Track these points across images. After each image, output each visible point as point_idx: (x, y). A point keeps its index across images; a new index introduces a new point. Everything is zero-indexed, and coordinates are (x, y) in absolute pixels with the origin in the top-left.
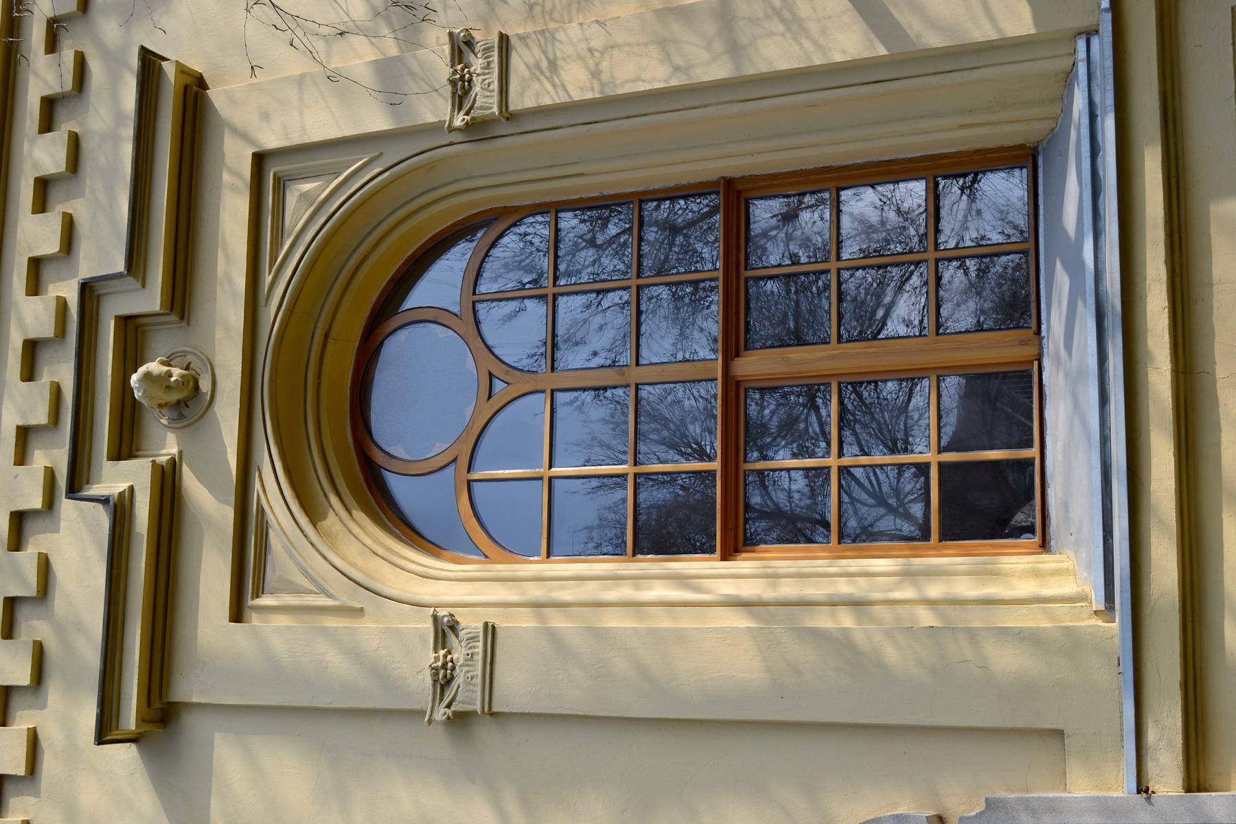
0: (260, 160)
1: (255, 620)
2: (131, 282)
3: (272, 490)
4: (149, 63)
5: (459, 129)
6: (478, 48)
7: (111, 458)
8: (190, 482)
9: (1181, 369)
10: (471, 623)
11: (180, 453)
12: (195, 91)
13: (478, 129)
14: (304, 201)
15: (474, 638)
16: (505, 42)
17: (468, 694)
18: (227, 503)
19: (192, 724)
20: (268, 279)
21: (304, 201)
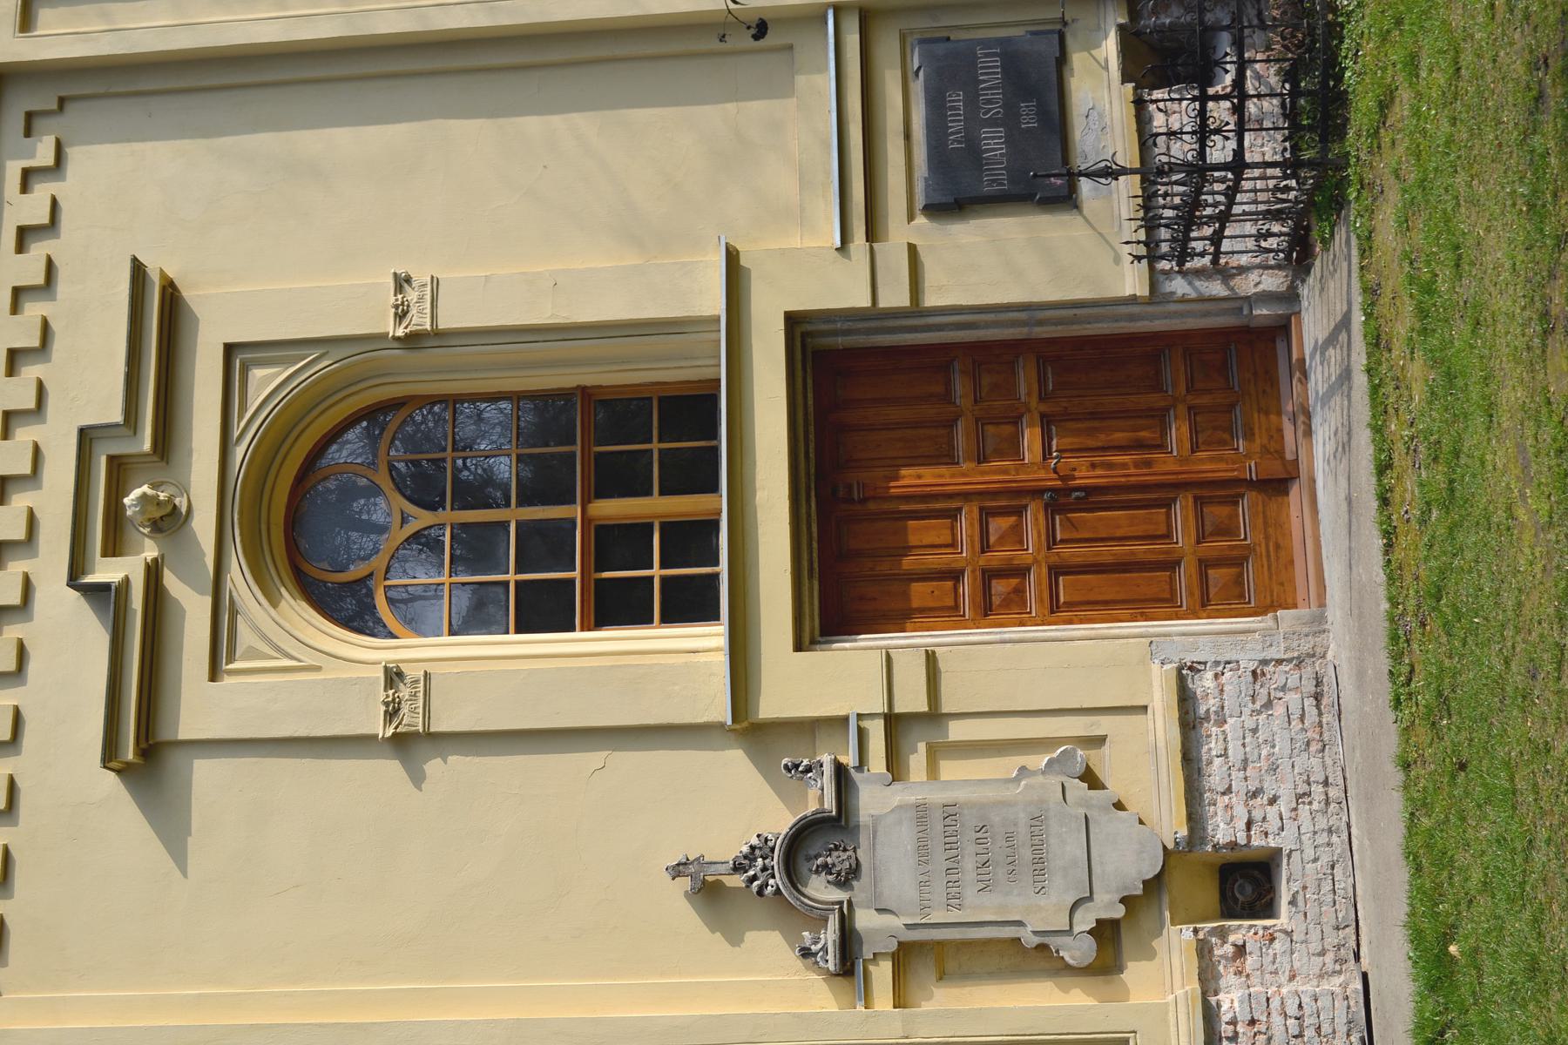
0: (230, 349)
1: (228, 681)
2: (125, 431)
3: (238, 578)
4: (138, 272)
5: (398, 339)
6: (408, 680)
7: (104, 555)
8: (170, 580)
9: (1301, 418)
10: (421, 276)
11: (163, 556)
12: (172, 297)
13: (413, 340)
14: (264, 381)
15: (417, 681)
16: (435, 283)
17: (411, 720)
18: (202, 593)
19: (175, 759)
20: (236, 434)
21: (264, 381)
